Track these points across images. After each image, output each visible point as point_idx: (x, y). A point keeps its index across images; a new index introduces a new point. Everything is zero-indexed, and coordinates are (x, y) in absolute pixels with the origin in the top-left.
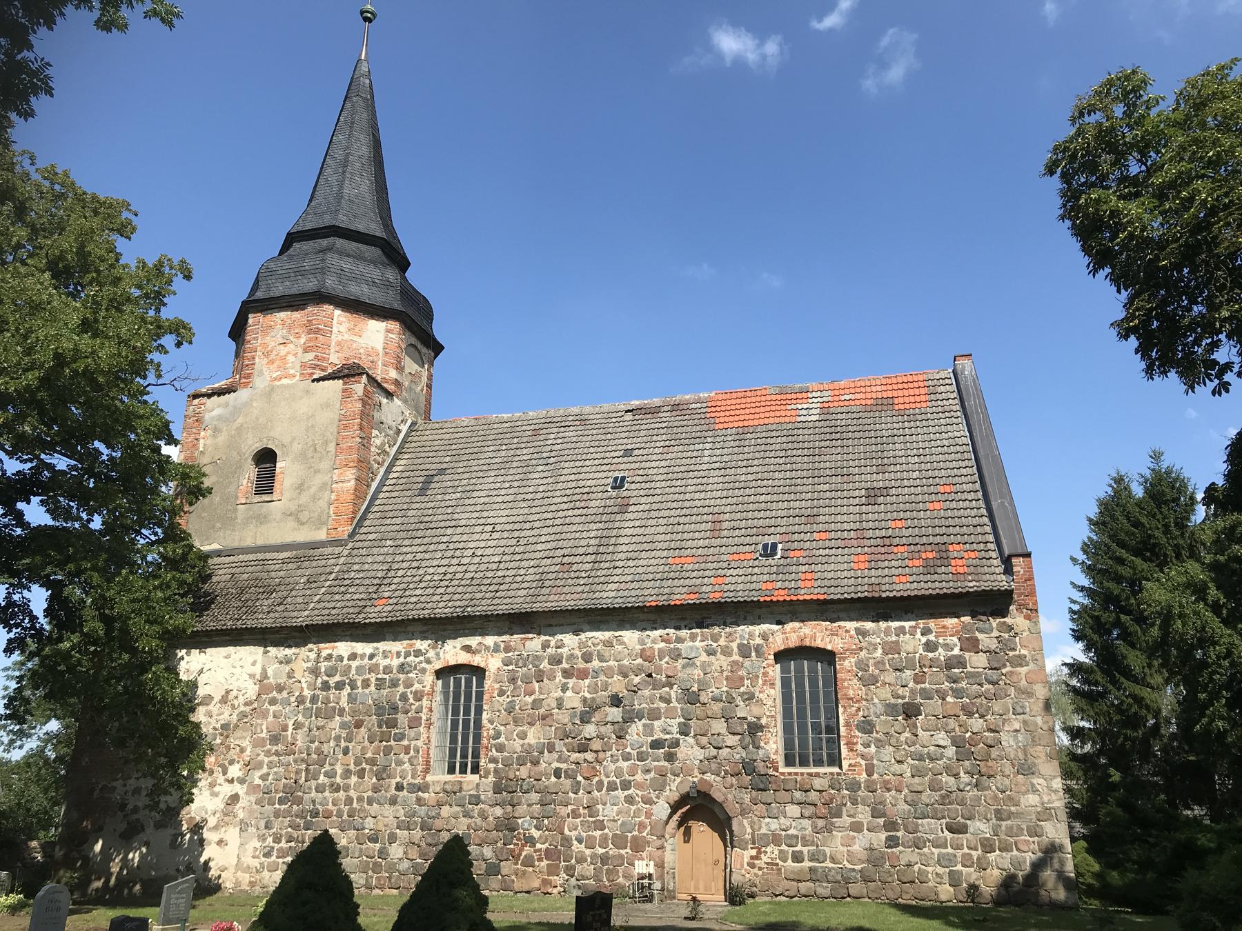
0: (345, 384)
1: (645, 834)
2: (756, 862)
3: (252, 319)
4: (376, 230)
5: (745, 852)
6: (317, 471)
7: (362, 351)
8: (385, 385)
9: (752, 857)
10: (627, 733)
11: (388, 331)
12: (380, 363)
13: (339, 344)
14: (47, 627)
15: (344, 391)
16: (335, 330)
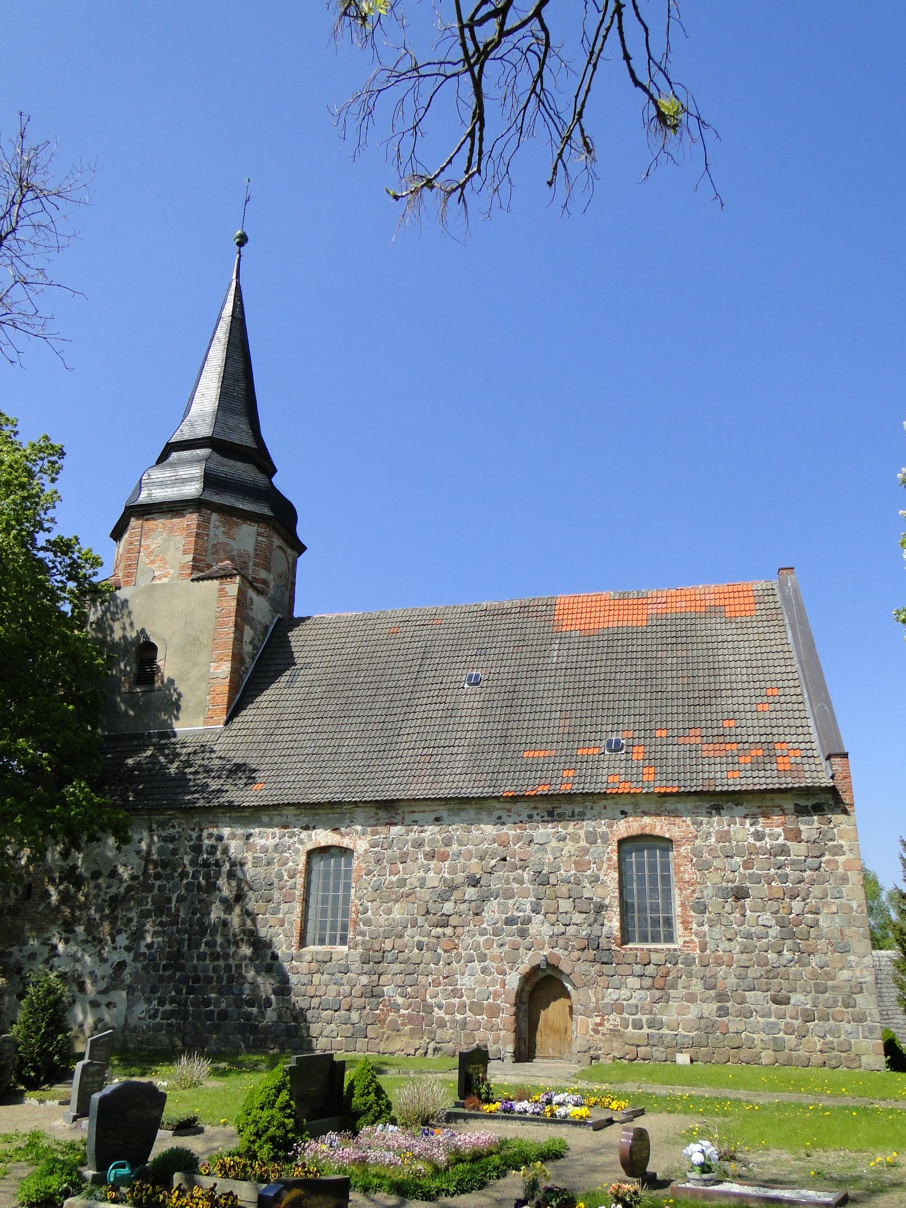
0: (221, 584)
1: (499, 1002)
2: (600, 1028)
3: (134, 522)
5: (590, 1020)
6: (195, 664)
7: (235, 553)
8: (254, 584)
9: (596, 1024)
10: (483, 910)
11: (259, 534)
12: (251, 564)
13: (214, 546)
15: (220, 590)
16: (211, 533)
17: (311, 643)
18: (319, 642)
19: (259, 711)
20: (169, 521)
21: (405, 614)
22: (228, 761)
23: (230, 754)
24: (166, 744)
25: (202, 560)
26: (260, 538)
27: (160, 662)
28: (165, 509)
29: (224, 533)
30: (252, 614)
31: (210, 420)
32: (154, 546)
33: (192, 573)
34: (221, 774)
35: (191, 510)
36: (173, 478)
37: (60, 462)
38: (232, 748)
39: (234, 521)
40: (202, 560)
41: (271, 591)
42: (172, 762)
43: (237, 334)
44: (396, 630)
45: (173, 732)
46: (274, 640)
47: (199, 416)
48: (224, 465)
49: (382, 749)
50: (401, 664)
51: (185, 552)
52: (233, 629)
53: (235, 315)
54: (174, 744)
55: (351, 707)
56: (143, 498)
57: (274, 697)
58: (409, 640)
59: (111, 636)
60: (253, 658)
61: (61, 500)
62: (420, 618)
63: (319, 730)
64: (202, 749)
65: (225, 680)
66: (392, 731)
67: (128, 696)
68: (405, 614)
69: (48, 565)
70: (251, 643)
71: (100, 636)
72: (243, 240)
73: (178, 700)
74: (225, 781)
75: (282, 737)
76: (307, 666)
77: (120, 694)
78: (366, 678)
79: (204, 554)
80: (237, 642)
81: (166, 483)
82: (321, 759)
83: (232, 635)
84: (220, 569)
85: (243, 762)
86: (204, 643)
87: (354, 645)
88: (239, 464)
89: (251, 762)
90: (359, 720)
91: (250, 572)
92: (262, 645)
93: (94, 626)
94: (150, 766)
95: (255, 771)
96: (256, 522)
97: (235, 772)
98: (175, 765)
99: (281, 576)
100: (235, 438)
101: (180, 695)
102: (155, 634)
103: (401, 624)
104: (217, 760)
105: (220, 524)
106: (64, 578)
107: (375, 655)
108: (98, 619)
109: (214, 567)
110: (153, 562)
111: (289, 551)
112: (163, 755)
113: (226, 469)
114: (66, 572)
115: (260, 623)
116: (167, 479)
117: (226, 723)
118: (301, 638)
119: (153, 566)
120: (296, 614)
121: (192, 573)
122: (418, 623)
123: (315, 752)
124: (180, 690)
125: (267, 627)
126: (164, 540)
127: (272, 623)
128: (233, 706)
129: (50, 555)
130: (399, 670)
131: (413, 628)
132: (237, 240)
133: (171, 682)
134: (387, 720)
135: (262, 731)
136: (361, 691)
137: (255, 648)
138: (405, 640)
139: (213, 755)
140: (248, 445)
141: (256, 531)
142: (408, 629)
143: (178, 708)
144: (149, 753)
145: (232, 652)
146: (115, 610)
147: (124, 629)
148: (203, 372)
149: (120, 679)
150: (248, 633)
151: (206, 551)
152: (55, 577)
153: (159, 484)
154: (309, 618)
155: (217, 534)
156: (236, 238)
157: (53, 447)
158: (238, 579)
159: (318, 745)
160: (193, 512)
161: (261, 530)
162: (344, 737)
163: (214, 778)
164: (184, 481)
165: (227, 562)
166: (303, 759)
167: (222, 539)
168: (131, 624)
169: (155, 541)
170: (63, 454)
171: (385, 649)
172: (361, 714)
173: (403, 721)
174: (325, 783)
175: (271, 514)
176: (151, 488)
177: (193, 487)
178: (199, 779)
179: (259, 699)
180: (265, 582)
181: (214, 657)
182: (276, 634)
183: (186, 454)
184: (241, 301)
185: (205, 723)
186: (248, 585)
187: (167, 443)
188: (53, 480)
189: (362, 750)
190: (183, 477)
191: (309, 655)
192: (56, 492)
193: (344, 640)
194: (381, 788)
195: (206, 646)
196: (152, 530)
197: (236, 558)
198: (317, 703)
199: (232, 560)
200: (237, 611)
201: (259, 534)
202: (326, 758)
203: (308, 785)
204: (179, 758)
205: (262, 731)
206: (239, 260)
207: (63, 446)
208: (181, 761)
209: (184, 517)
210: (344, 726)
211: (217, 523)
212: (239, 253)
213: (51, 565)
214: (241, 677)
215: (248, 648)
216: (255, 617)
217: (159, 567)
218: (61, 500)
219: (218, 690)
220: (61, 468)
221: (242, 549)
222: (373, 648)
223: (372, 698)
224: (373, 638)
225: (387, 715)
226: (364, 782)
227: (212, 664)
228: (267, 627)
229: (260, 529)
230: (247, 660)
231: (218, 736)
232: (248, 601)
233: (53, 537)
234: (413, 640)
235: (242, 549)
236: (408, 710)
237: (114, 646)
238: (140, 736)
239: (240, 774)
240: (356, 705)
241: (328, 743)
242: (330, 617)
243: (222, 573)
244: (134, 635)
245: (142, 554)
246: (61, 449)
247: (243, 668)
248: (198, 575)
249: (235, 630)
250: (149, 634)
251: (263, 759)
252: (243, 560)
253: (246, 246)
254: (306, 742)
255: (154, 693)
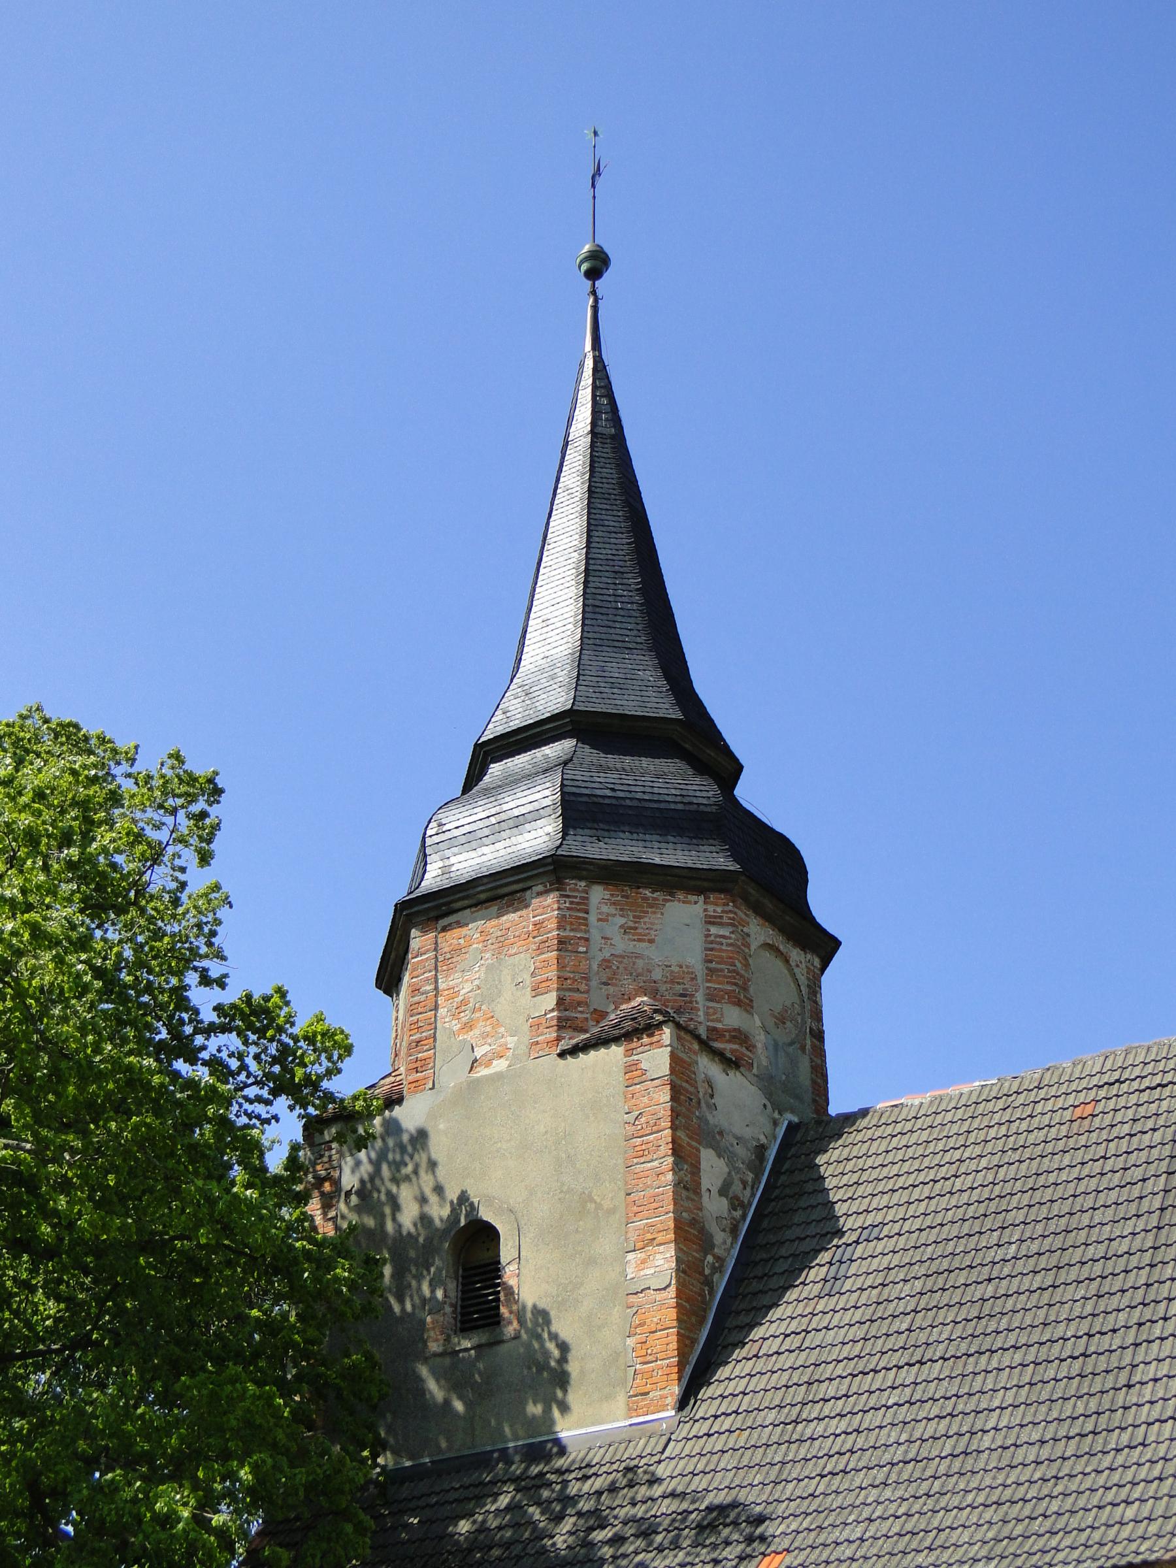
0: (629, 1053)
3: (419, 940)
4: (663, 706)
6: (591, 1262)
7: (657, 975)
8: (717, 1045)
11: (710, 921)
12: (699, 997)
13: (606, 964)
14: (189, 1093)
15: (630, 1068)
16: (595, 935)
17: (875, 1174)
18: (895, 1169)
19: (760, 1365)
20: (494, 922)
21: (1108, 1065)
22: (693, 1502)
23: (699, 1483)
24: (541, 1475)
25: (579, 1004)
26: (714, 930)
27: (510, 1274)
28: (483, 896)
29: (626, 930)
30: (716, 1119)
31: (566, 674)
32: (468, 987)
33: (559, 1039)
34: (678, 1536)
35: (540, 888)
36: (493, 820)
37: (214, 811)
38: (700, 1467)
39: (645, 899)
40: (579, 1004)
41: (762, 1056)
42: (559, 1518)
43: (609, 472)
44: (1089, 1109)
45: (557, 1442)
46: (783, 1179)
47: (542, 671)
48: (606, 769)
49: (1089, 1427)
50: (1113, 1195)
51: (537, 991)
52: (670, 1160)
53: (599, 430)
54: (559, 1472)
55: (993, 1325)
56: (432, 879)
57: (794, 1323)
58: (1126, 1129)
59: (394, 1219)
60: (734, 1231)
61: (231, 907)
62: (1149, 1068)
63: (917, 1397)
64: (630, 1476)
65: (664, 1294)
66: (1111, 1377)
67: (447, 1361)
68: (1108, 1065)
69: (227, 1066)
70: (723, 1192)
71: (370, 1222)
72: (598, 263)
73: (563, 1360)
74: (688, 1554)
75: (823, 1424)
76: (870, 1233)
77: (426, 1360)
78: (1024, 1246)
79: (583, 987)
80: (684, 1193)
81: (480, 834)
82: (929, 1473)
83: (670, 1176)
84: (624, 1019)
85: (729, 1499)
86: (607, 1204)
87: (984, 1163)
88: (645, 762)
89: (751, 1499)
90: (1018, 1357)
91: (701, 1021)
92: (753, 1195)
93: (354, 1199)
94: (508, 1534)
95: (760, 1520)
96: (700, 891)
97: (712, 1527)
98: (568, 1524)
99: (781, 1020)
100: (629, 705)
101: (564, 1347)
102: (490, 1200)
103: (1102, 1093)
104: (667, 1501)
105: (612, 910)
106: (265, 1093)
107: (1041, 1180)
108: (362, 1182)
109: (612, 1016)
110: (468, 1026)
111: (795, 955)
112: (538, 1504)
113: (612, 777)
114: (268, 1076)
115: (739, 1139)
116: (481, 824)
117: (682, 1404)
118: (850, 1166)
119: (471, 1036)
120: (833, 1110)
121: (559, 1039)
122: (1146, 1083)
123: (911, 1455)
124: (565, 1334)
125: (761, 1150)
126: (490, 968)
127: (775, 1138)
128: (693, 1359)
129: (232, 1041)
130: (1110, 1211)
131: (1133, 1099)
132: (584, 267)
133: (543, 1316)
134: (1092, 1349)
135: (772, 1416)
136: (1016, 1281)
137: (736, 1203)
138: (1115, 1132)
139: (658, 1490)
140: (661, 714)
141: (702, 915)
142: (1122, 1102)
143: (562, 1379)
144: (504, 1501)
145: (675, 1219)
146: (398, 1157)
147: (423, 1200)
148: (542, 571)
149: (422, 1322)
150: (712, 1168)
151: (587, 979)
152: (247, 1092)
153: (463, 839)
154: (864, 1113)
155: (609, 935)
156: (582, 262)
157: (192, 779)
158: (667, 1034)
159: (917, 1435)
160: (547, 892)
161: (715, 909)
162: (983, 1405)
163: (660, 1549)
164: (519, 822)
165: (639, 1000)
166: (881, 1477)
167: (621, 944)
168: (439, 1190)
169: (467, 976)
170: (218, 791)
171: (1066, 1162)
172: (1023, 1341)
173: (1137, 1345)
174: (943, 1535)
175: (733, 866)
176: (448, 853)
177: (540, 832)
178: (624, 1556)
179: (757, 1333)
180: (740, 1037)
181: (633, 1236)
182: (786, 1166)
183: (521, 761)
184: (609, 387)
185: (632, 1410)
186: (696, 1046)
187: (476, 745)
188: (205, 858)
189: (1035, 1436)
190: (516, 812)
191: (874, 1205)
192: (217, 887)
193: (957, 1155)
194: (1097, 1536)
195: (612, 1211)
196: (458, 950)
197: (663, 988)
198: (904, 1326)
199: (654, 993)
200: (675, 1114)
201: (710, 921)
202: (942, 1469)
203: (901, 1546)
204: (574, 1506)
205: (772, 1416)
206: (595, 309)
207: (216, 773)
208: (580, 1514)
209: (527, 906)
210: (979, 1378)
211: (605, 909)
212: (594, 292)
213: (234, 1064)
214: (708, 1283)
215: (715, 1206)
216: (725, 1124)
217: (484, 1036)
218: (231, 907)
219: (653, 1320)
220: (216, 827)
221: (674, 962)
222: (1035, 1163)
223: (1047, 1294)
224: (1031, 1138)
225: (1090, 1336)
226: (1048, 1523)
227: (630, 1256)
228: (761, 1150)
229: (711, 908)
230: (719, 1237)
231: (664, 1439)
232: (702, 1089)
233: (230, 996)
234: (1138, 1127)
235: (674, 962)
236: (1148, 1313)
237: (401, 1245)
238: (483, 1461)
239: (726, 1532)
240: (1005, 1320)
241: (942, 1429)
242: (917, 1102)
243: (628, 1025)
244: (446, 1212)
245: (442, 1011)
246: (210, 781)
247: (710, 1258)
248: (574, 1041)
249: (675, 1163)
250: (476, 1201)
251: (780, 1487)
252: (679, 988)
253: (606, 275)
254: (885, 1431)
255: (504, 1348)
